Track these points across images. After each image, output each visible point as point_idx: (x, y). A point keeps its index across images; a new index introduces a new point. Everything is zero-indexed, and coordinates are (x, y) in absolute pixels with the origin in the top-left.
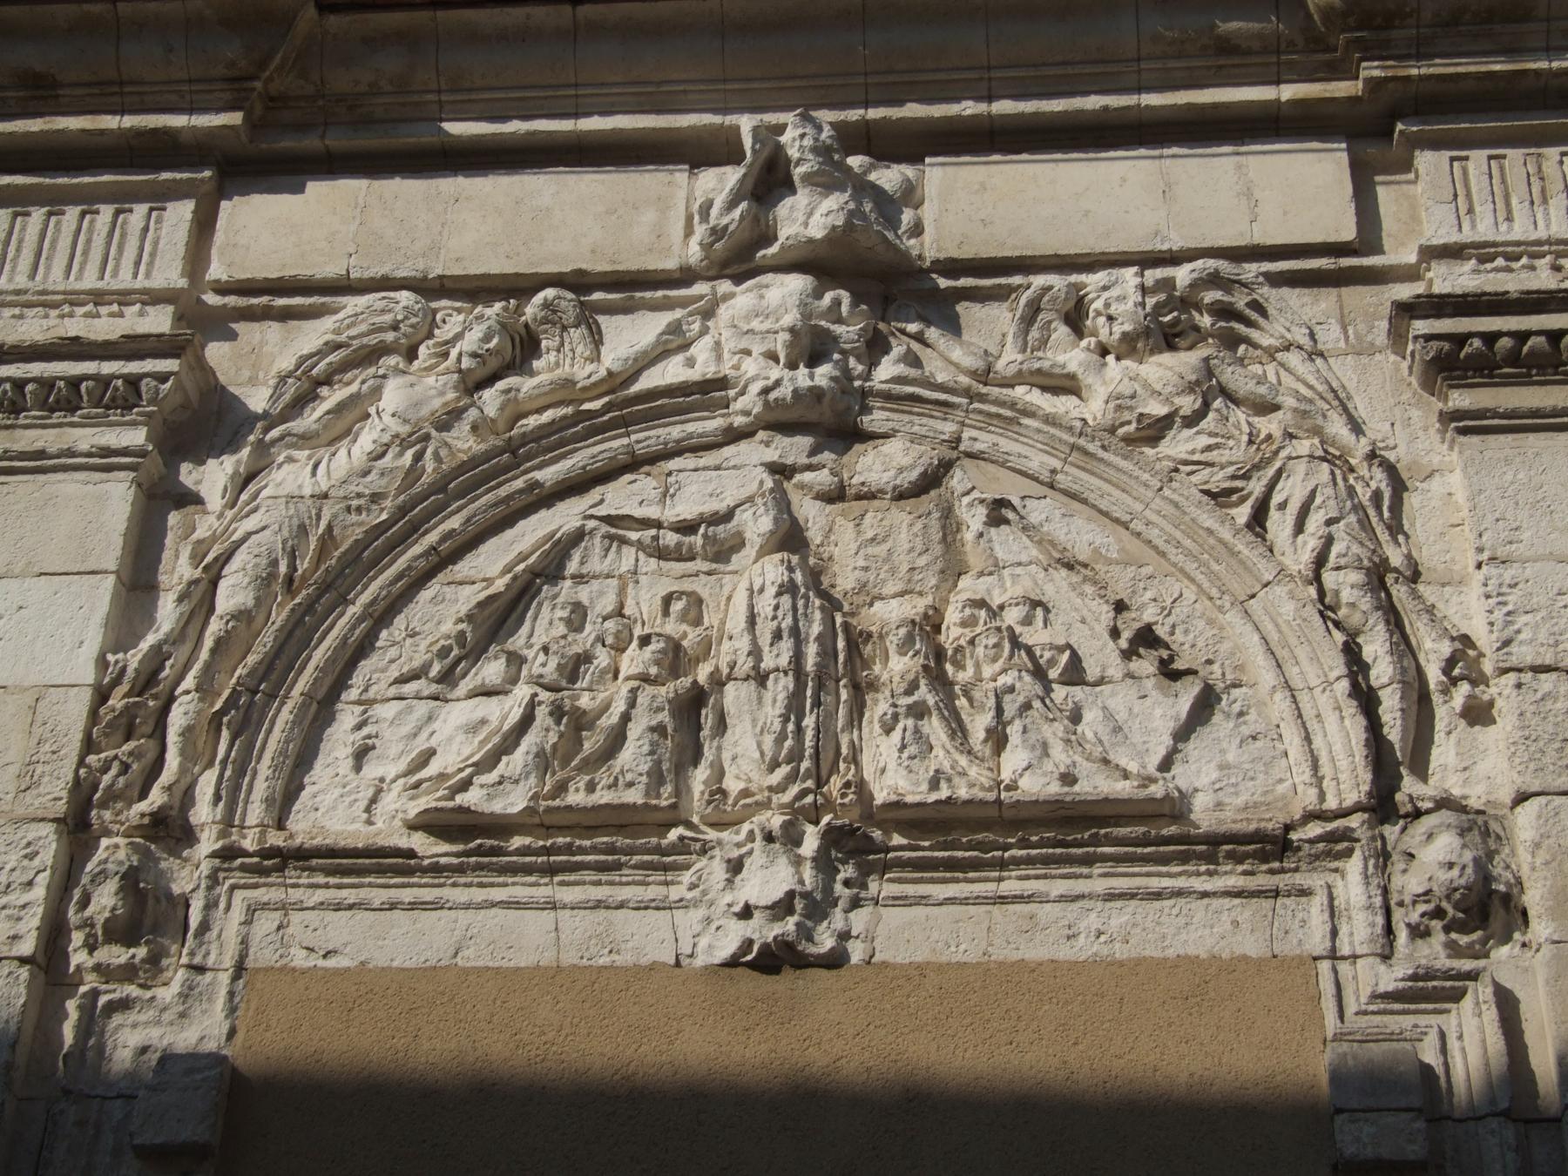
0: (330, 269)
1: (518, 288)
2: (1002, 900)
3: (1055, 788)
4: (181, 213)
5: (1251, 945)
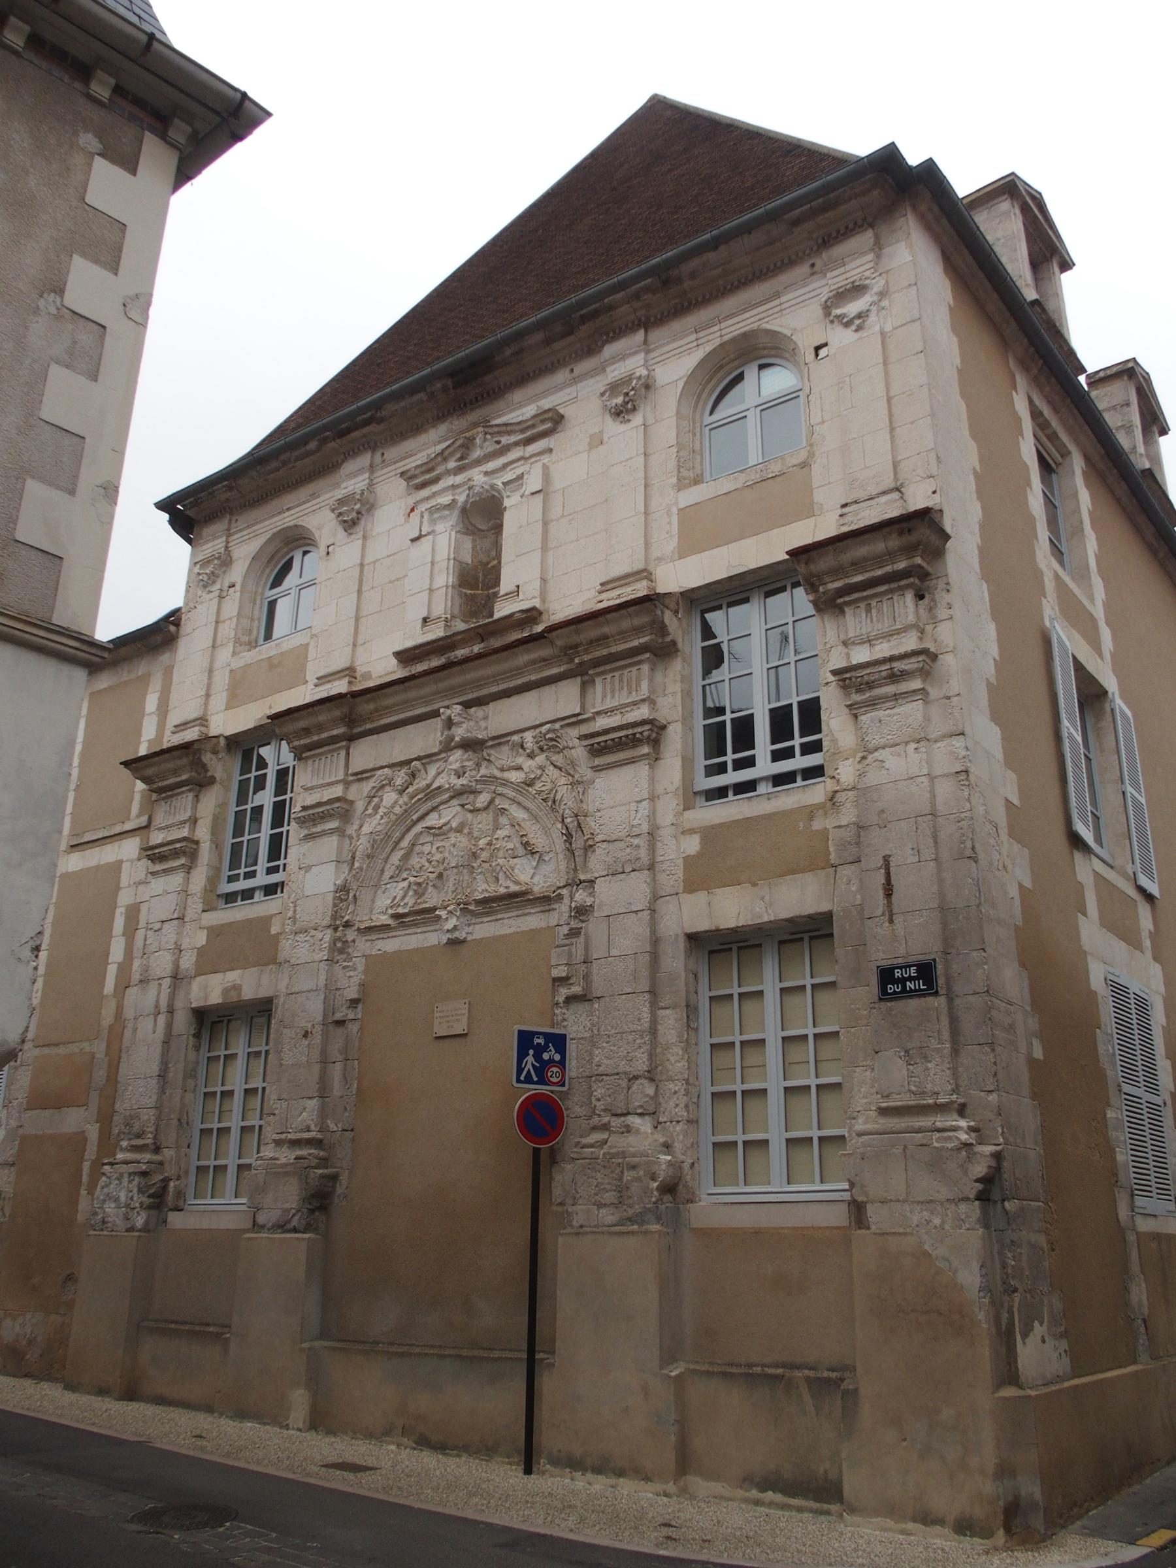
0: (370, 766)
1: (408, 762)
2: (497, 920)
3: (505, 890)
4: (343, 753)
5: (544, 925)
